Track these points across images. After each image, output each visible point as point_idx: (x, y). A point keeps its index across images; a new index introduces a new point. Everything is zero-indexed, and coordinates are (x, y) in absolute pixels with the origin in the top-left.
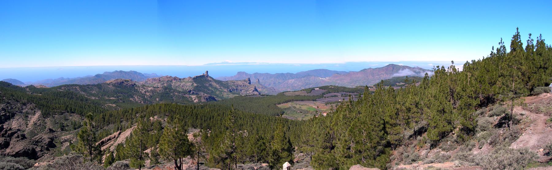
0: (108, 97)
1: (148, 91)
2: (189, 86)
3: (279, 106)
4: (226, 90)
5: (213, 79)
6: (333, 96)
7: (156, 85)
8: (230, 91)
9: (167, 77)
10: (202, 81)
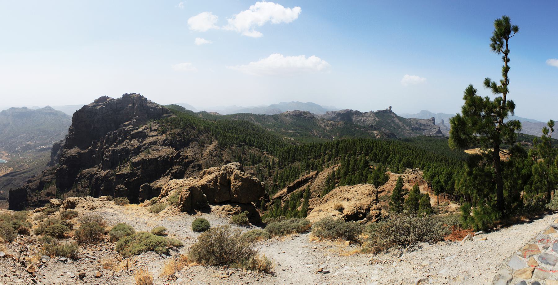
0: (285, 129)
1: (328, 125)
2: (370, 120)
4: (407, 128)
8: (412, 130)
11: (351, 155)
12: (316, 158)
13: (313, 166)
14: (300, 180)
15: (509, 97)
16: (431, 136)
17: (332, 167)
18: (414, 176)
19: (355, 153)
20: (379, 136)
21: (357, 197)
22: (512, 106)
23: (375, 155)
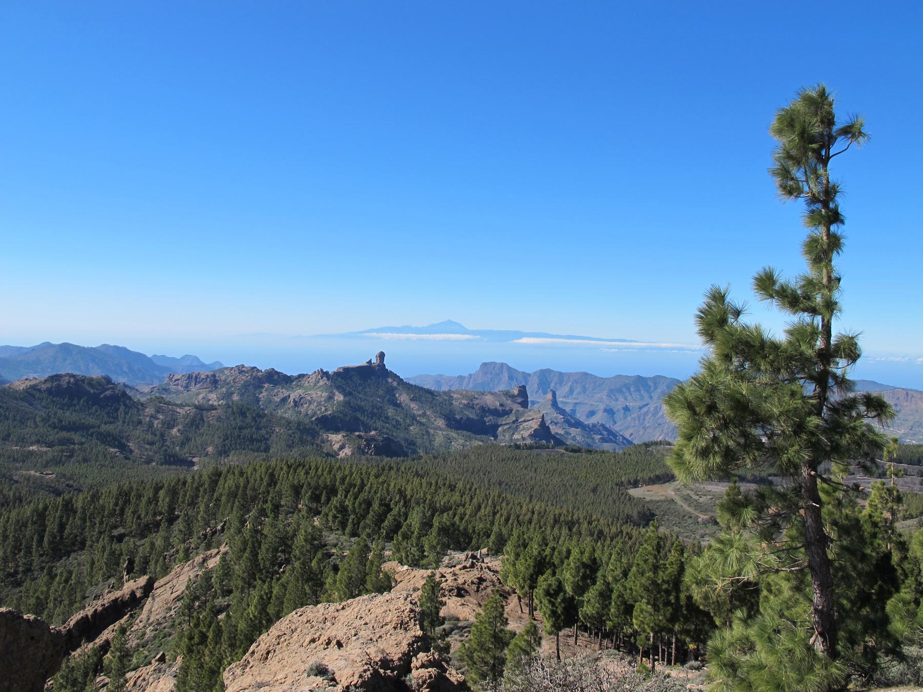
2: (319, 401)
3: (634, 492)
5: (400, 381)
6: (600, 340)
7: (199, 400)
9: (241, 370)
10: (366, 384)
11: (263, 513)
12: (145, 530)
13: (131, 562)
14: (89, 611)
15: (839, 328)
16: (517, 447)
17: (199, 559)
18: (474, 574)
19: (277, 507)
20: (347, 451)
21: (365, 633)
22: (850, 350)
23: (343, 510)
